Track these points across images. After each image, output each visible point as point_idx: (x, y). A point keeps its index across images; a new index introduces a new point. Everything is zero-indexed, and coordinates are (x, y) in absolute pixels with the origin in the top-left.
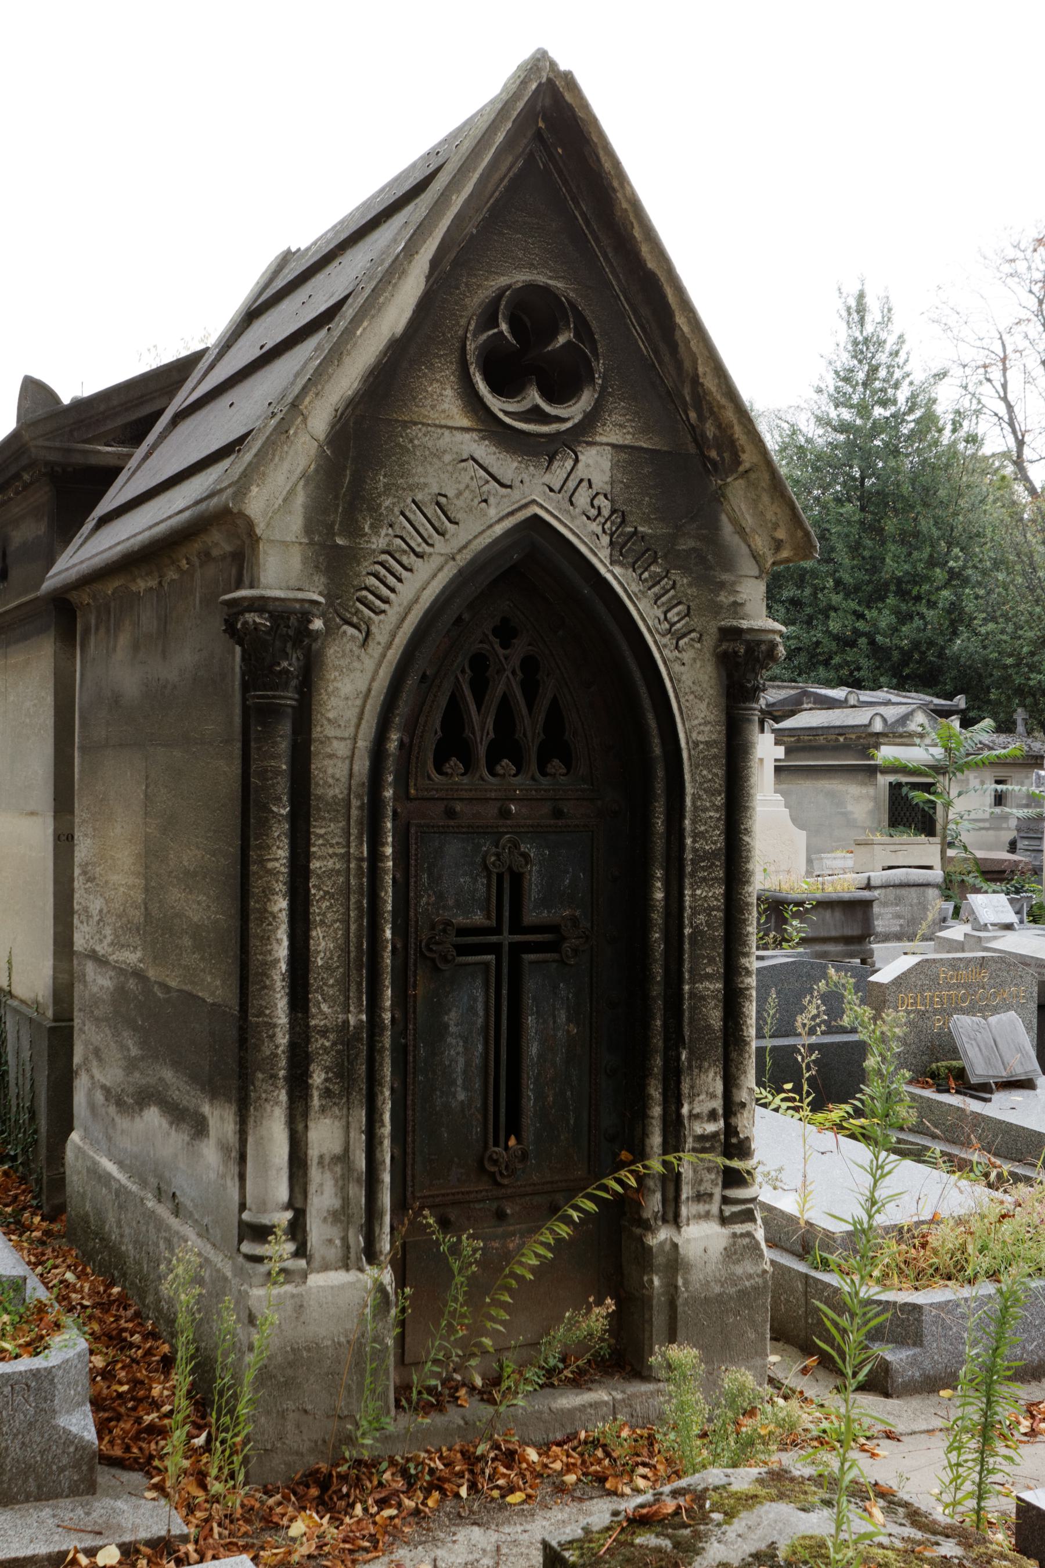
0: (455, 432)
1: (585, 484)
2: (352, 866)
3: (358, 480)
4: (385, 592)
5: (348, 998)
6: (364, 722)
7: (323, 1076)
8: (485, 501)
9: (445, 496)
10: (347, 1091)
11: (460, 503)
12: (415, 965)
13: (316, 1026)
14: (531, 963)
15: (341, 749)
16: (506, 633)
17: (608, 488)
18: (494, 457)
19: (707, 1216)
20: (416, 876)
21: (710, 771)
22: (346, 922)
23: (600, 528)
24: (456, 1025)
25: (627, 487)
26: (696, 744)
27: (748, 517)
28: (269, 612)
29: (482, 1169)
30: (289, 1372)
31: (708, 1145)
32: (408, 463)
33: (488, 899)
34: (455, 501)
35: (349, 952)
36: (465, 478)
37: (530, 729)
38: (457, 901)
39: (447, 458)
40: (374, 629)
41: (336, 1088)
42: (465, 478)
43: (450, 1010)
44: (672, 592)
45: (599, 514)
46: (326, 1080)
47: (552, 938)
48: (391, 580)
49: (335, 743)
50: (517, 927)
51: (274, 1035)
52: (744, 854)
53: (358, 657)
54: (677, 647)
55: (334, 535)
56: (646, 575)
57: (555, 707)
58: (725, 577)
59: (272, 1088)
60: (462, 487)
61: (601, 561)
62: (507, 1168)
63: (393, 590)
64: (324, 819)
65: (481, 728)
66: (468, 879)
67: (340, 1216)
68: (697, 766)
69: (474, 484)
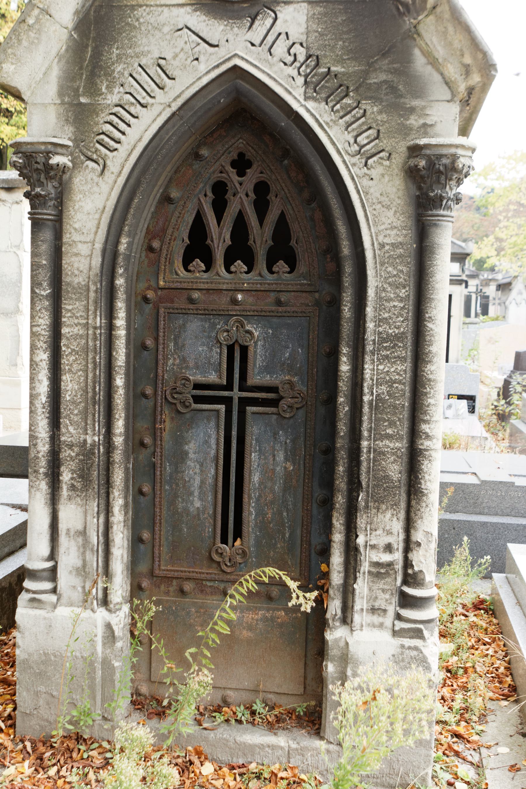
0: (172, 9)
1: (283, 36)
2: (90, 332)
3: (97, 54)
4: (117, 135)
5: (86, 424)
6: (100, 230)
7: (70, 476)
8: (197, 59)
9: (164, 59)
10: (86, 487)
11: (176, 63)
12: (161, 407)
13: (65, 441)
14: (253, 413)
15: (84, 249)
16: (241, 165)
17: (303, 38)
18: (204, 24)
19: (381, 626)
21: (395, 268)
22: (86, 371)
23: (296, 71)
24: (195, 453)
25: (321, 35)
26: (382, 246)
27: (439, 48)
28: (22, 153)
29: (211, 559)
30: (42, 667)
31: (383, 571)
32: (135, 37)
33: (220, 364)
34: (172, 62)
35: (87, 393)
36: (180, 43)
37: (261, 238)
38: (196, 363)
39: (166, 29)
40: (108, 163)
41: (78, 485)
42: (180, 43)
43: (190, 442)
44: (363, 119)
45: (295, 60)
46: (72, 479)
48: (122, 126)
49: (80, 245)
51: (36, 444)
52: (428, 338)
53: (97, 184)
54: (366, 165)
55: (79, 96)
56: (338, 107)
57: (282, 219)
58: (416, 103)
59: (35, 479)
60: (178, 50)
61: (295, 98)
63: (123, 133)
64: (71, 298)
65: (220, 237)
66: (205, 348)
67: (82, 571)
68: (382, 264)
69: (187, 47)
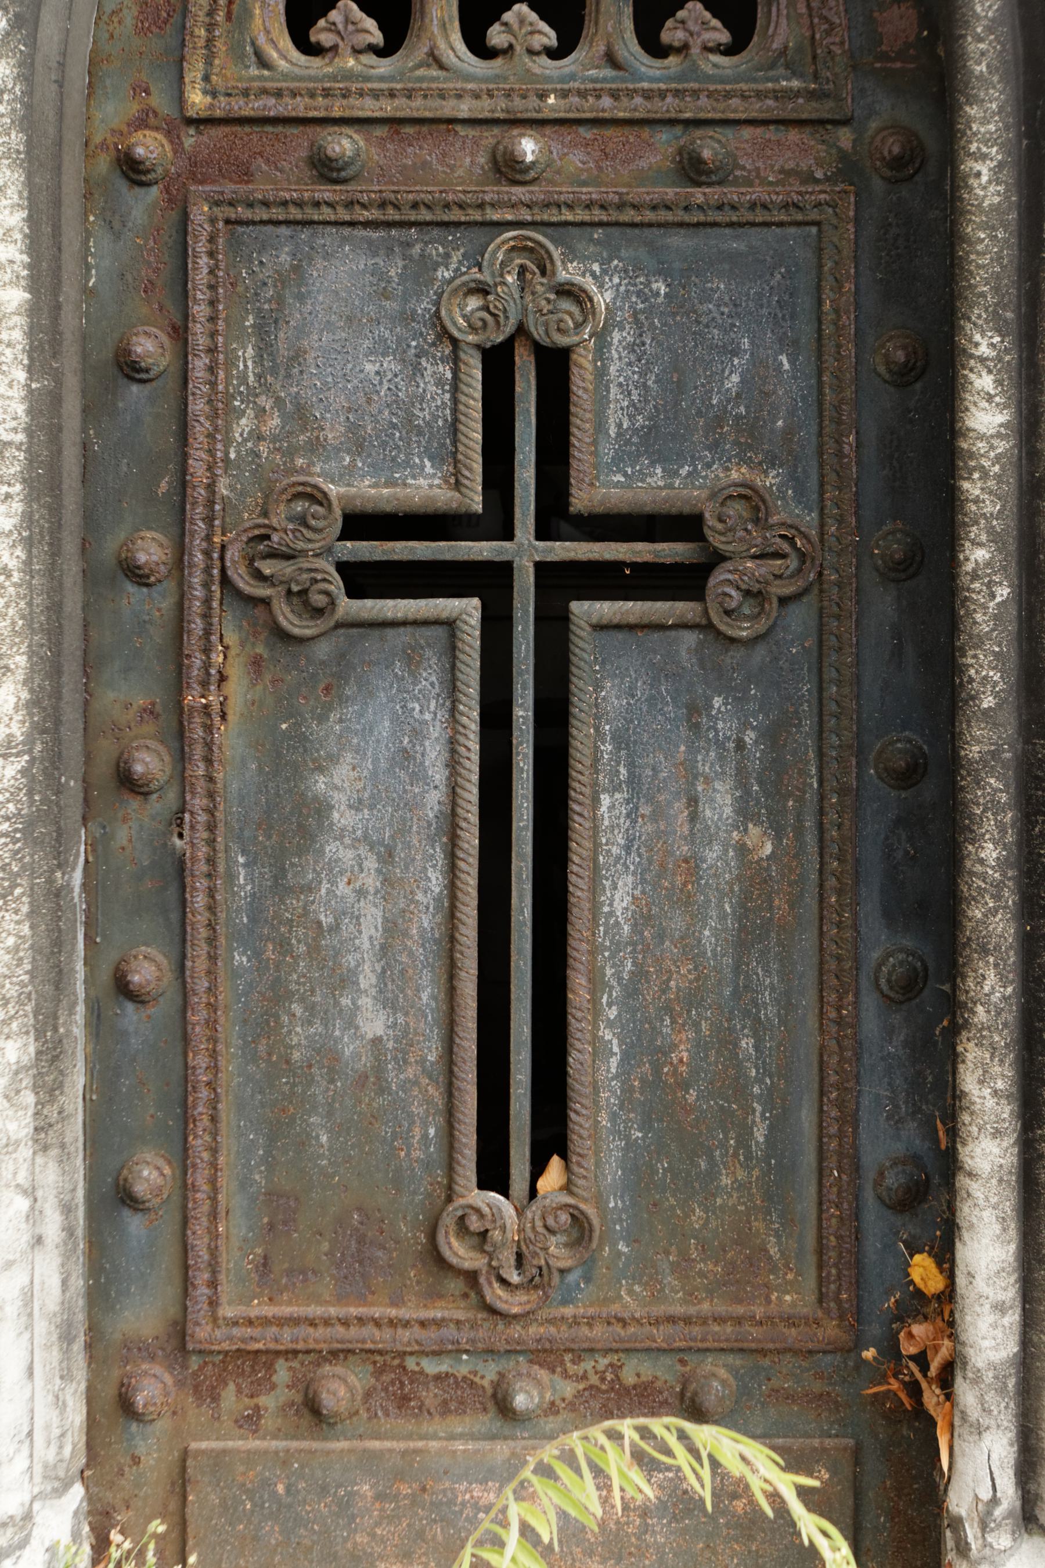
14: (600, 627)
20: (212, 350)
24: (357, 806)
38: (353, 428)
43: (334, 759)
47: (668, 560)
62: (520, 1259)
66: (390, 364)
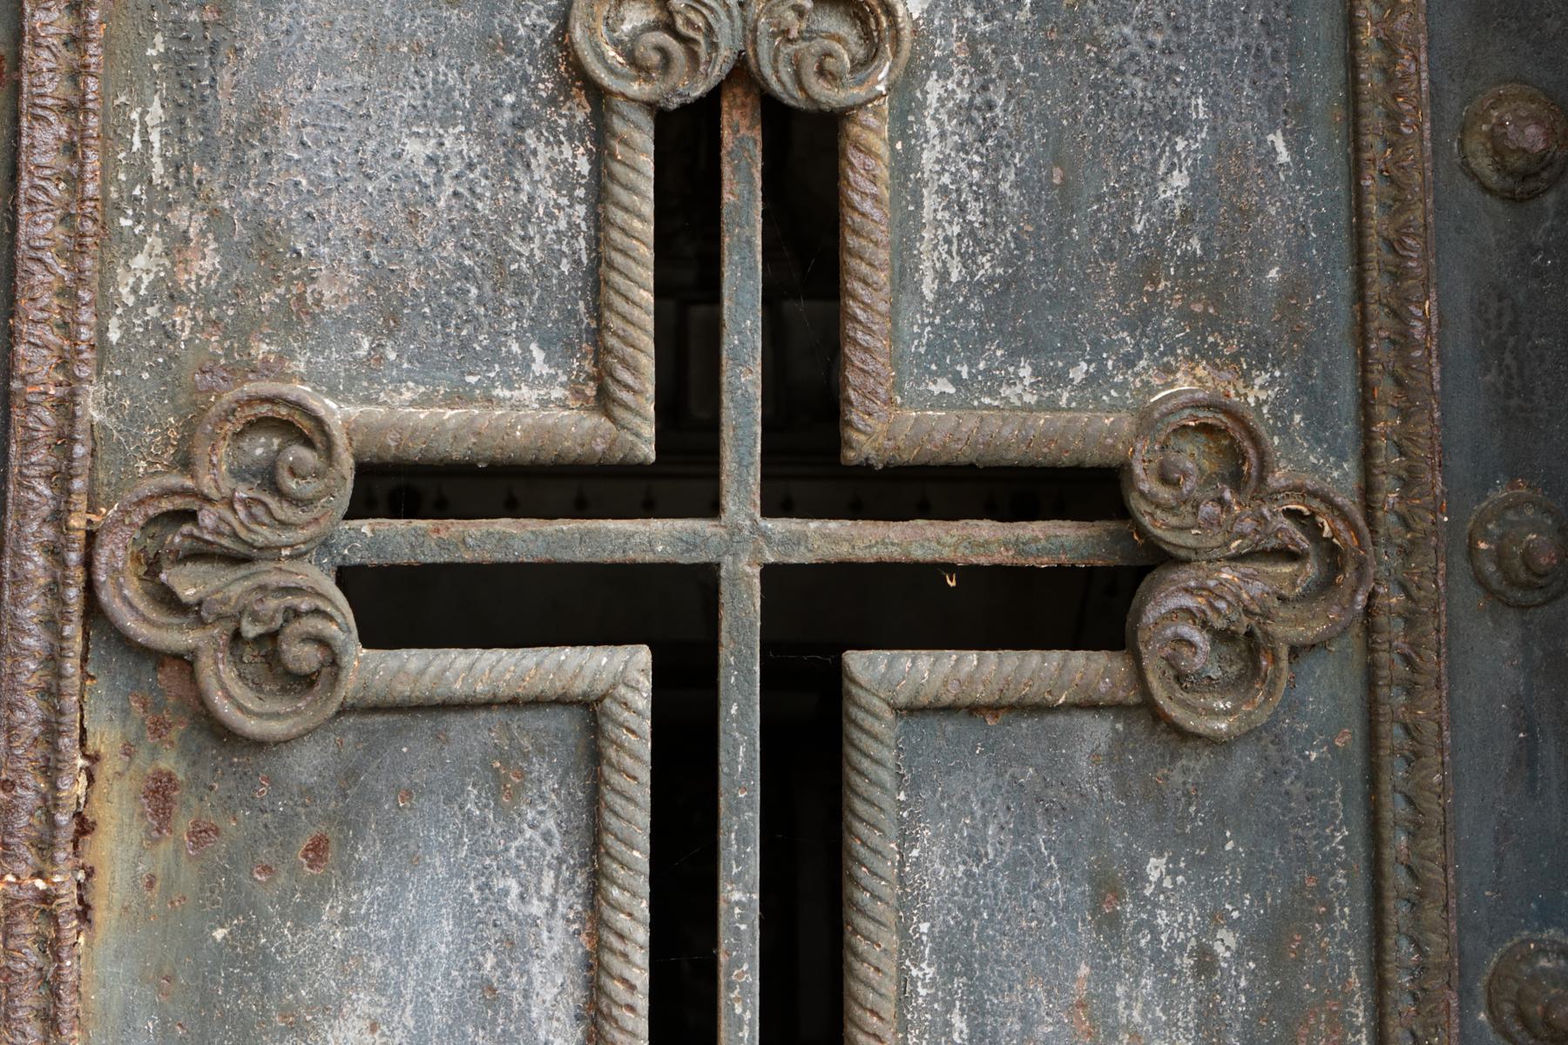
14: (911, 711)
20: (74, 109)
38: (378, 278)
47: (1066, 567)
50: (811, 459)
66: (458, 142)
